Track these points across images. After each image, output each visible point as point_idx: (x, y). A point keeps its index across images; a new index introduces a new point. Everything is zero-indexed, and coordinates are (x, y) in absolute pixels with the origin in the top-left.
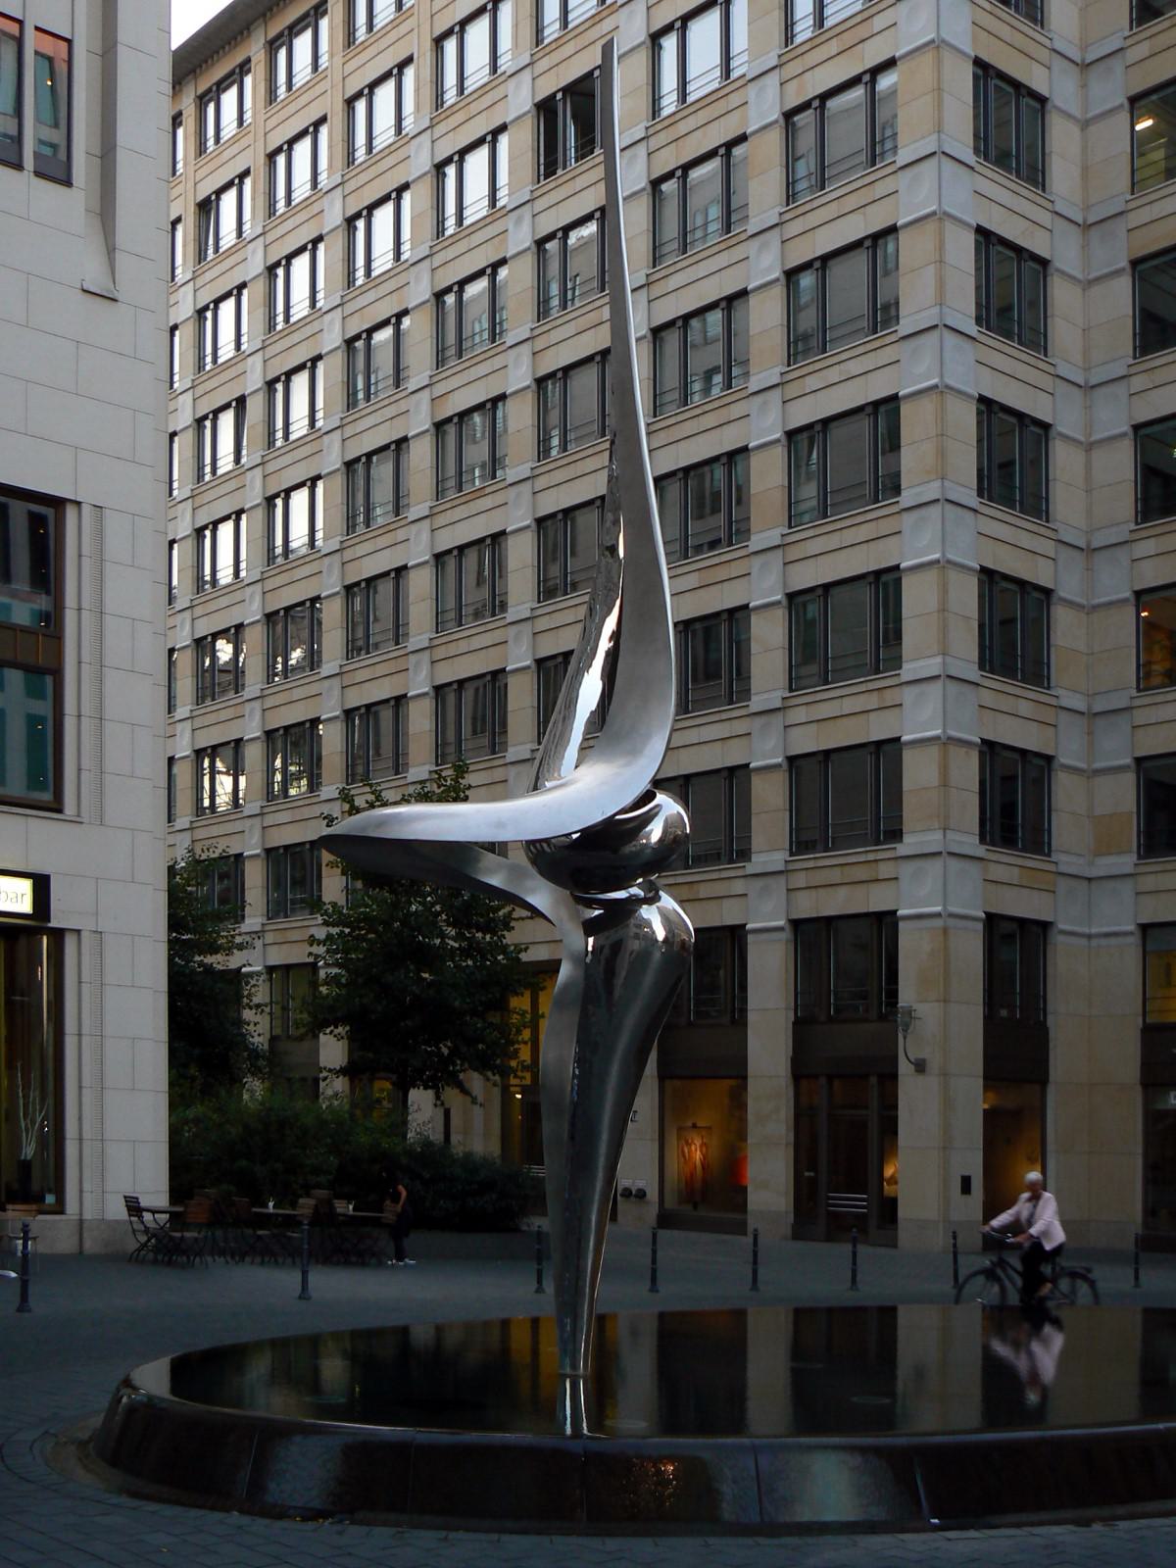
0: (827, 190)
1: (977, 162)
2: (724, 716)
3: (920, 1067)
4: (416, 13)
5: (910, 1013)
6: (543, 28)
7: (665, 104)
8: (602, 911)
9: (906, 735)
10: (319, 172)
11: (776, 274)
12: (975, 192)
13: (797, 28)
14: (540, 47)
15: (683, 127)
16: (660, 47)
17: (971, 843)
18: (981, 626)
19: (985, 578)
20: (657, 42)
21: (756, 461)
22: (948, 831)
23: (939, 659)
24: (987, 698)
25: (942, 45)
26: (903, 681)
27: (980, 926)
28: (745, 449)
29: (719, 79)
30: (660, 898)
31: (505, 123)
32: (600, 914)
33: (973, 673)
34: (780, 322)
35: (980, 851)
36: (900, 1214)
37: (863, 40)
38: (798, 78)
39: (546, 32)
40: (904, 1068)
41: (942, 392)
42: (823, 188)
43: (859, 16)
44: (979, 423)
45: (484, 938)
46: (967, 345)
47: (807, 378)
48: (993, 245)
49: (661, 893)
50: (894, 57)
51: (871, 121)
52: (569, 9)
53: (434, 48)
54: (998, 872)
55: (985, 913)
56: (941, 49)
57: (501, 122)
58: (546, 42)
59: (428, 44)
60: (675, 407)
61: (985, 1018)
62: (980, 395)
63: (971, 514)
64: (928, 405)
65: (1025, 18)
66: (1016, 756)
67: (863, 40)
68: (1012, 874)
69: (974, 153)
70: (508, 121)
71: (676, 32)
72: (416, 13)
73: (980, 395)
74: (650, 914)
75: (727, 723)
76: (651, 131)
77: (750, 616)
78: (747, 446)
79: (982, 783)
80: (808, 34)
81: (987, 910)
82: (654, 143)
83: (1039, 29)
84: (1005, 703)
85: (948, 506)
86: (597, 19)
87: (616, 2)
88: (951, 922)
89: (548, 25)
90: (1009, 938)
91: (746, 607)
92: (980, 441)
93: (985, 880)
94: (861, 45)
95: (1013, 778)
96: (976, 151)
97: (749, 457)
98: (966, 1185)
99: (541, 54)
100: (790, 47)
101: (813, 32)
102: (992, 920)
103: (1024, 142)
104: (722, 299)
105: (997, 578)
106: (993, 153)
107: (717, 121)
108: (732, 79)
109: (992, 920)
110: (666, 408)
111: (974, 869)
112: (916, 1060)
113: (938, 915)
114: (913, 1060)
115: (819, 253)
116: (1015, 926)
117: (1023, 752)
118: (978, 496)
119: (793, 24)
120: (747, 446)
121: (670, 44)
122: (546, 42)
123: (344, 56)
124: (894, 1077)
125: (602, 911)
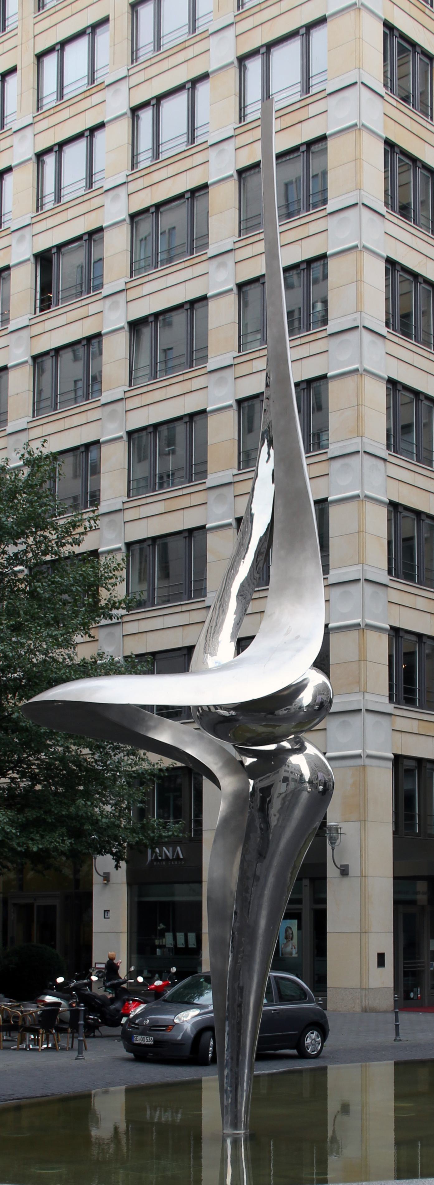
0: (195, 255)
1: (387, 212)
2: (185, 608)
3: (344, 871)
4: (20, 35)
5: (337, 830)
6: (42, 98)
7: (46, 202)
8: (255, 760)
9: (333, 623)
10: (5, 115)
11: (232, 285)
12: (386, 233)
13: (248, 110)
14: (40, 112)
15: (156, 177)
16: (138, 117)
17: (382, 703)
18: (389, 543)
19: (391, 509)
20: (243, 64)
21: (212, 421)
22: (365, 693)
23: (359, 567)
24: (395, 596)
25: (363, 128)
26: (330, 583)
27: (390, 764)
28: (204, 412)
29: (53, 202)
30: (305, 748)
31: (103, 122)
32: (254, 762)
33: (384, 577)
34: (124, 356)
35: (390, 708)
36: (330, 983)
37: (301, 122)
38: (250, 146)
39: (45, 102)
40: (332, 872)
41: (361, 374)
42: (192, 254)
43: (299, 104)
44: (388, 395)
45: (57, 788)
46: (379, 341)
47: (254, 361)
48: (398, 271)
49: (307, 744)
50: (102, 226)
51: (88, 259)
52: (65, 85)
53: (130, 11)
54: (401, 724)
55: (393, 754)
56: (362, 131)
57: (8, 165)
58: (45, 109)
59: (31, 59)
60: (147, 380)
61: (395, 833)
62: (388, 377)
63: (381, 463)
64: (350, 382)
65: (419, 112)
66: (414, 638)
67: (301, 122)
68: (413, 726)
69: (385, 206)
70: (13, 165)
71: (85, 138)
72: (20, 35)
73: (388, 377)
74: (297, 760)
75: (187, 614)
76: (130, 178)
77: (206, 534)
78: (206, 409)
79: (390, 657)
80: (148, 163)
81: (395, 752)
82: (132, 187)
83: (429, 120)
84: (407, 600)
85: (366, 457)
86: (88, 94)
87: (103, 82)
88: (368, 762)
89: (142, 47)
90: (409, 772)
91: (203, 527)
92: (388, 408)
93: (393, 730)
94: (299, 125)
95: (413, 653)
96: (386, 204)
97: (207, 418)
98: (381, 959)
99: (41, 117)
100: (243, 124)
101: (54, 204)
102: (398, 759)
103: (420, 198)
104: (186, 302)
105: (400, 509)
106: (397, 208)
107: (47, 228)
108: (62, 202)
109: (398, 759)
110: (139, 381)
111: (384, 721)
112: (342, 866)
113: (359, 756)
114: (339, 866)
115: (188, 298)
116: (413, 764)
117: (420, 636)
118: (387, 449)
119: (245, 107)
120: (206, 409)
121: (146, 116)
122: (45, 109)
123: (35, 18)
124: (323, 879)
125: (255, 760)
